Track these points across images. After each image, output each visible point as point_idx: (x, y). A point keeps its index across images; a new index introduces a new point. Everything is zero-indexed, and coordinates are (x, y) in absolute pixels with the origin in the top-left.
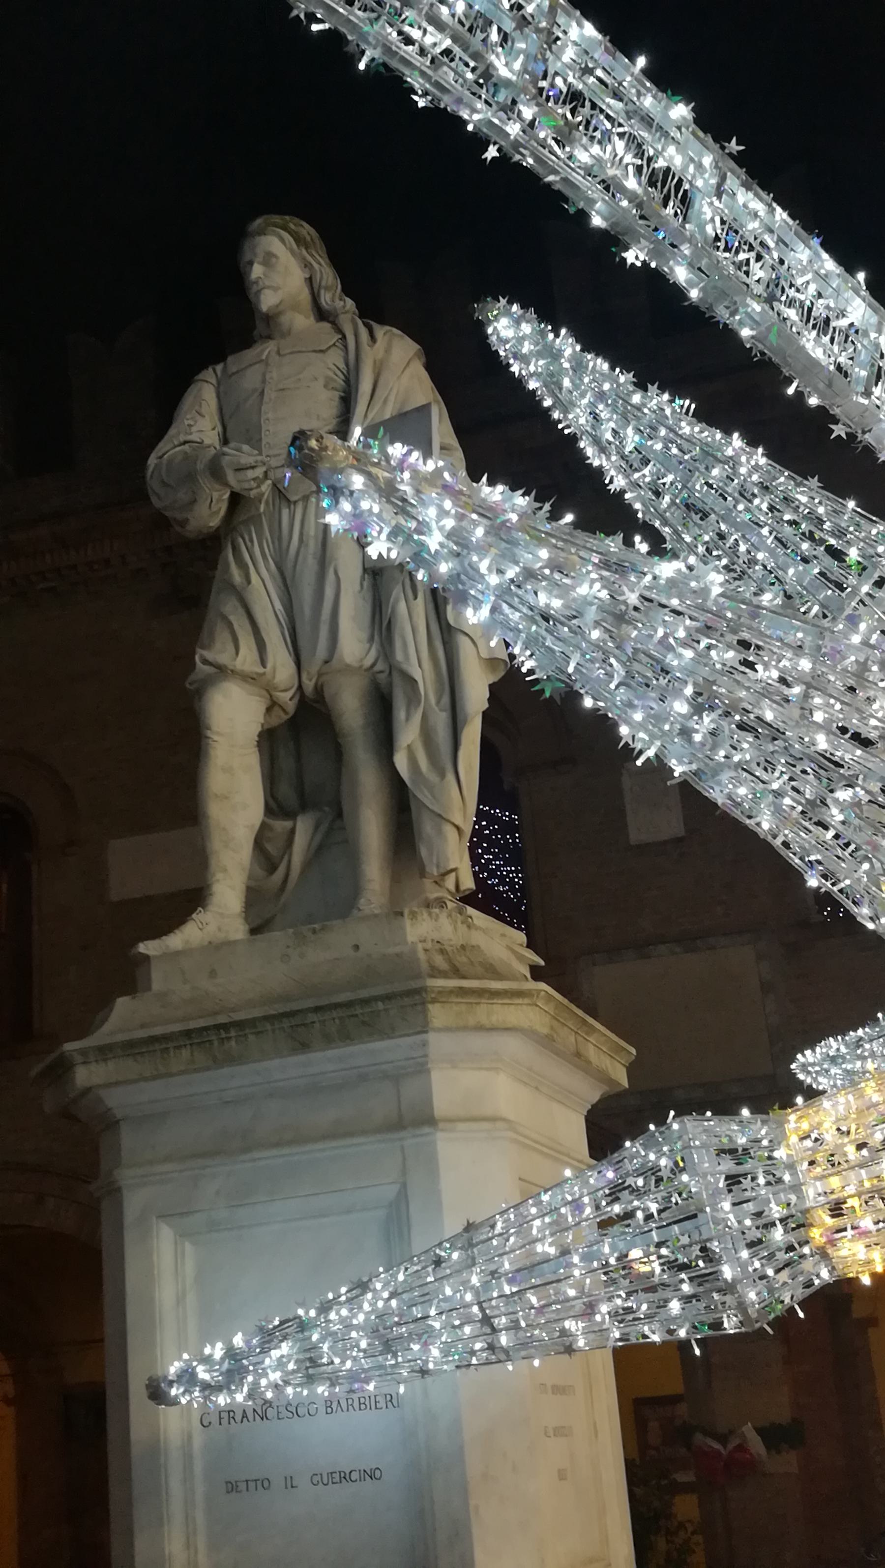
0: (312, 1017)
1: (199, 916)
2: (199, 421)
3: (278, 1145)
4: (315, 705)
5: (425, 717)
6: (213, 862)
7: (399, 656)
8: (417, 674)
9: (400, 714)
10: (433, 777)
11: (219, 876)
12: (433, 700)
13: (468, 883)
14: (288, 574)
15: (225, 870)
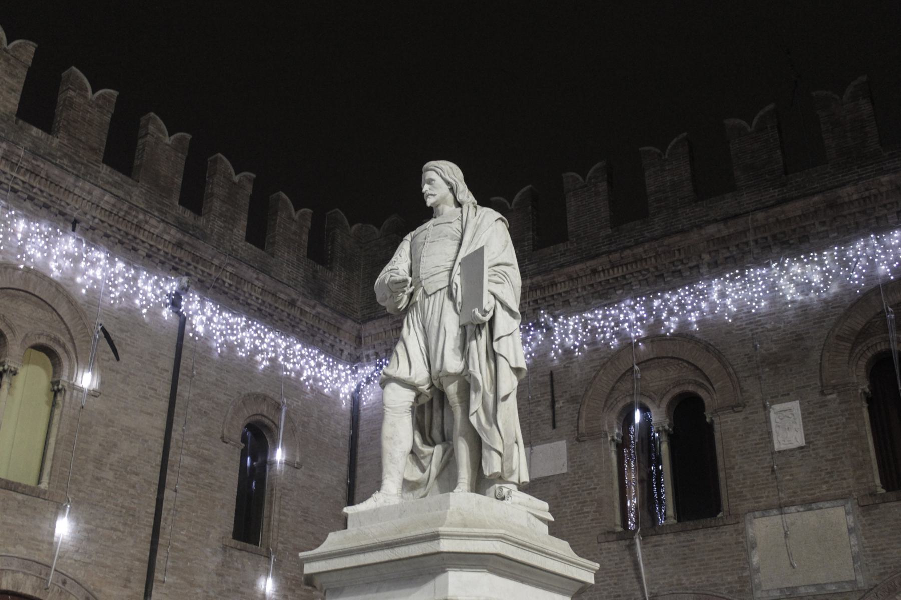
0: (285, 281)
1: (377, 496)
2: (400, 264)
3: (400, 560)
4: (459, 299)
5: (483, 398)
6: (385, 470)
7: (471, 369)
8: (479, 377)
9: (473, 396)
10: (487, 427)
11: (387, 476)
12: (487, 388)
13: (525, 478)
14: (427, 327)
15: (390, 473)
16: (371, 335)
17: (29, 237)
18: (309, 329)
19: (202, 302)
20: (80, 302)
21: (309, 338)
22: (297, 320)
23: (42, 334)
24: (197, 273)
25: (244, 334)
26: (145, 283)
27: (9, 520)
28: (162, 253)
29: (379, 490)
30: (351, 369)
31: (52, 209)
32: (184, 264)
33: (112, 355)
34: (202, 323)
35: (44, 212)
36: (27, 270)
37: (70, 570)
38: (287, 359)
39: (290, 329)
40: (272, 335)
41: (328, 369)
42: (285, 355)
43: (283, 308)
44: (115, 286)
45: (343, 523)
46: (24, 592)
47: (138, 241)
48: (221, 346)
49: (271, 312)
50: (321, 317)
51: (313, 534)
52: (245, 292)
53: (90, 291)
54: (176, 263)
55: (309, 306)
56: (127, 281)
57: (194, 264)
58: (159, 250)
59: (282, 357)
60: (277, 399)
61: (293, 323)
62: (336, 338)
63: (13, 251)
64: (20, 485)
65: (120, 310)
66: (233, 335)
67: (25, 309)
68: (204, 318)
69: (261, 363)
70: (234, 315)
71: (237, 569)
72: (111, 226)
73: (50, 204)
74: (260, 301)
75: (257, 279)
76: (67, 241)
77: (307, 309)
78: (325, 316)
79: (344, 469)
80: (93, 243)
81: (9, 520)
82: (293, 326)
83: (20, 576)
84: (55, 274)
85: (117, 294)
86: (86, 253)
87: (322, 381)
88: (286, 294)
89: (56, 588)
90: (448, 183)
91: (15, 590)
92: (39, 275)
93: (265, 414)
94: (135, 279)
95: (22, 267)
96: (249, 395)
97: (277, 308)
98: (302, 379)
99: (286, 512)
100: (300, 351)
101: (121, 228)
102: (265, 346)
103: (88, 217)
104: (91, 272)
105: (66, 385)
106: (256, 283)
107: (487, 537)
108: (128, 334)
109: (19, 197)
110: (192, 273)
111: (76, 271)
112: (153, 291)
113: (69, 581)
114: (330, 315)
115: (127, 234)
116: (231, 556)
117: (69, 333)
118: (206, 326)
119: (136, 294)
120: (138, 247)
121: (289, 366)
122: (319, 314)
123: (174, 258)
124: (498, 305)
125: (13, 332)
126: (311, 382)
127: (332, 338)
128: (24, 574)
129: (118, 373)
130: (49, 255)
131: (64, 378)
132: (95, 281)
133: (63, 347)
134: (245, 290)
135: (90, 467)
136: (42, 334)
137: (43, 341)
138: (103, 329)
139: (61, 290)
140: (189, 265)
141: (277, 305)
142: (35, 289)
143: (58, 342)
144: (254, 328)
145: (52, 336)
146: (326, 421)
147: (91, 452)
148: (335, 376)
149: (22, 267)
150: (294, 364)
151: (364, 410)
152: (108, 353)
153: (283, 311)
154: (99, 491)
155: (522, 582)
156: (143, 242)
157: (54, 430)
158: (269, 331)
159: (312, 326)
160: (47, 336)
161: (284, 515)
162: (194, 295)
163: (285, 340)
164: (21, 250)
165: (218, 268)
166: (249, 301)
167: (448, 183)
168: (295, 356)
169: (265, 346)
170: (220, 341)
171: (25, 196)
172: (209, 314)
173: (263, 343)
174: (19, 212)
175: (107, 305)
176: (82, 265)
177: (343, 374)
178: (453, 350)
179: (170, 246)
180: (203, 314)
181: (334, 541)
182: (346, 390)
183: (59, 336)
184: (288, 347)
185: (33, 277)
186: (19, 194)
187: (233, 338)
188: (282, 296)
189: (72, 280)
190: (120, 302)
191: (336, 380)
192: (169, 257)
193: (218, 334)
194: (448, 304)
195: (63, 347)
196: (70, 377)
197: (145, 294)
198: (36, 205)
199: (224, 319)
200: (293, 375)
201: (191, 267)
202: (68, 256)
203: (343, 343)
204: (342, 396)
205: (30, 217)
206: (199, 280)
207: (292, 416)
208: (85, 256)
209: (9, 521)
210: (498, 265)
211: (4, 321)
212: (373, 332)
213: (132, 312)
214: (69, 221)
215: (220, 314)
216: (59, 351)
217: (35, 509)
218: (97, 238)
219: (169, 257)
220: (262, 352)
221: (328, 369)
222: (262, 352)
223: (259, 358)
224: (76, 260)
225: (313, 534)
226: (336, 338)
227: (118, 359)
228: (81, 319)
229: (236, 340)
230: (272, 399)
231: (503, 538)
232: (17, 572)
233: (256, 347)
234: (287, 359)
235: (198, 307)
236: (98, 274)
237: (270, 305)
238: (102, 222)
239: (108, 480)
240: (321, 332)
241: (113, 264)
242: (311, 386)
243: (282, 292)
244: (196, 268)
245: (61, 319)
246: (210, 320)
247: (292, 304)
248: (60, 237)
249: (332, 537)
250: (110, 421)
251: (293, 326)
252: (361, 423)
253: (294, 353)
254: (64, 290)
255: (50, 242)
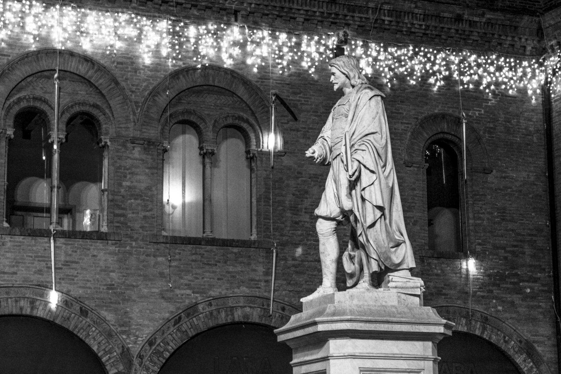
15: (325, 274)
16: (551, 25)
17: (200, 39)
18: (481, 37)
19: (366, 46)
20: (254, 80)
21: (483, 47)
22: (467, 33)
23: (228, 116)
24: (354, 21)
25: (413, 62)
26: (308, 45)
27: (231, 269)
28: (318, 14)
29: (321, 284)
30: (537, 62)
31: (214, 9)
32: (340, 17)
33: (290, 117)
34: (368, 65)
35: (209, 12)
36: (204, 67)
37: (286, 299)
38: (462, 73)
39: (462, 42)
40: (442, 55)
41: (511, 69)
42: (459, 70)
43: (449, 26)
44: (281, 57)
45: (299, 308)
46: (253, 321)
47: (293, 11)
48: (391, 80)
49: (437, 33)
50: (493, 22)
51: (512, 230)
52: (406, 23)
53: (260, 68)
54: (334, 18)
55: (478, 16)
56: (291, 48)
57: (351, 14)
58: (315, 12)
59: (457, 73)
60: (457, 114)
61: (463, 37)
62: (513, 37)
63: (190, 55)
64: (233, 240)
65: (290, 75)
66: (402, 66)
67: (210, 99)
68: (370, 59)
69: (435, 85)
70: (400, 48)
71: (437, 275)
72: (266, 6)
73: (210, 5)
74: (424, 27)
75: (416, 7)
76: (232, 31)
77: (476, 19)
78: (497, 20)
79: (542, 162)
80: (255, 25)
81: (231, 269)
82: (464, 39)
83: (248, 310)
84: (228, 63)
85: (285, 63)
86: (250, 36)
87: (505, 83)
88: (450, 12)
89: (277, 315)
90: (344, 74)
91: (246, 320)
92: (215, 69)
93: (446, 131)
94: (298, 45)
95: (199, 66)
96: (425, 118)
97: (443, 28)
98: (481, 88)
99: (481, 216)
100: (475, 61)
101: (276, 5)
102: (436, 68)
103: (245, 5)
104: (258, 52)
105: (256, 152)
106: (416, 11)
107: (342, 321)
108: (301, 95)
109: (185, 8)
110: (351, 22)
111: (245, 54)
112: (317, 51)
113: (287, 308)
114: (503, 18)
115: (283, 8)
116: (429, 264)
117: (250, 109)
118: (373, 66)
119: (301, 58)
120: (296, 16)
121: (466, 79)
122: (489, 19)
123: (331, 14)
124: (362, 167)
125: (203, 120)
126: (493, 87)
127: (509, 38)
128: (251, 307)
129: (298, 130)
130: (220, 49)
131: (253, 147)
132: (263, 59)
133: (247, 121)
134: (406, 21)
135: (288, 214)
136: (228, 116)
137: (230, 121)
138: (278, 97)
139: (236, 75)
140: (346, 16)
141: (441, 25)
142: (214, 81)
143: (241, 118)
144: (422, 54)
145: (237, 115)
146: (514, 122)
147: (287, 202)
148: (520, 74)
149: (199, 66)
150: (471, 75)
151: (555, 101)
152: (287, 116)
153: (450, 29)
154: (299, 232)
155: (382, 339)
156: (299, 10)
157: (254, 190)
158: (439, 52)
159: (485, 33)
160: (233, 116)
161: (479, 218)
162: (356, 41)
163: (456, 56)
164: (196, 52)
165: (375, 10)
166: (413, 30)
167: (344, 74)
168: (470, 67)
169: (436, 68)
170: (388, 76)
171: (189, 6)
172: (374, 54)
173: (434, 64)
174: (187, 21)
175: (278, 75)
176: (249, 48)
177: (529, 70)
178: (346, 195)
179: (325, 5)
180: (368, 56)
181: (294, 319)
182: (533, 86)
183: (242, 114)
184: (461, 62)
185: (211, 71)
186: (184, 6)
187: (402, 70)
188: (446, 15)
189: (244, 63)
190: (289, 69)
191: (521, 79)
192: (325, 15)
193: (386, 69)
194: (341, 164)
195: (247, 121)
196: (258, 145)
197: (309, 55)
198: (199, 10)
199: (391, 54)
200: (471, 86)
201: (348, 18)
202: (235, 44)
203: (523, 40)
204: (530, 92)
205: (199, 20)
206: (359, 26)
207: (475, 125)
208: (249, 40)
209: (231, 270)
210: (367, 135)
211: (196, 114)
212: (552, 22)
213: (302, 75)
214: (231, 13)
215: (386, 50)
216: (245, 125)
217: (249, 257)
218: (258, 19)
219: (325, 15)
220: (434, 74)
221: (511, 69)
222: (434, 74)
223: (432, 80)
224: (243, 46)
225: (512, 230)
226: (513, 37)
227: (296, 119)
228: (257, 94)
229: (406, 70)
230: (451, 115)
231: (351, 320)
232: (245, 307)
233: (427, 71)
234: (462, 73)
235: (362, 52)
236: (264, 51)
237: (436, 27)
238: (259, 5)
239: (305, 222)
240: (496, 36)
241: (275, 38)
242: (493, 92)
243: (444, 12)
244: (353, 17)
245: (242, 99)
246: (376, 59)
247: (459, 19)
248: (225, 30)
249: (293, 318)
250: (299, 173)
251: (464, 39)
252: (554, 114)
253: (470, 64)
254: (238, 74)
255: (217, 36)
